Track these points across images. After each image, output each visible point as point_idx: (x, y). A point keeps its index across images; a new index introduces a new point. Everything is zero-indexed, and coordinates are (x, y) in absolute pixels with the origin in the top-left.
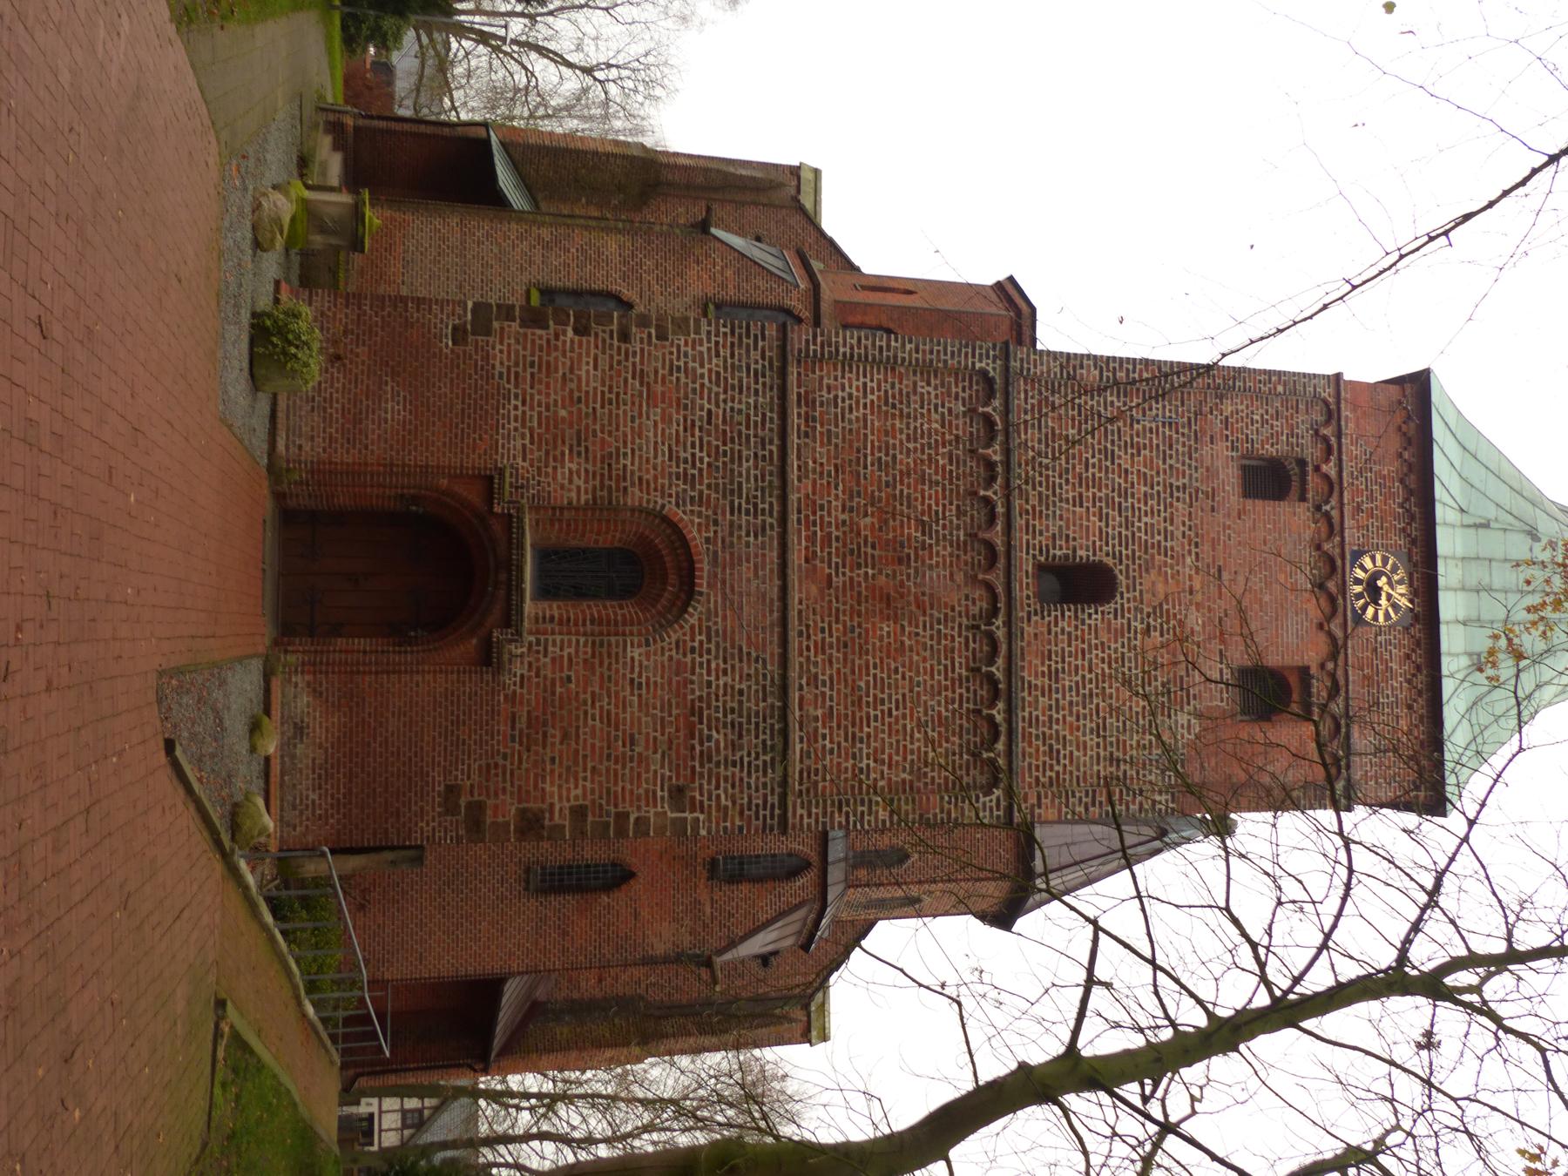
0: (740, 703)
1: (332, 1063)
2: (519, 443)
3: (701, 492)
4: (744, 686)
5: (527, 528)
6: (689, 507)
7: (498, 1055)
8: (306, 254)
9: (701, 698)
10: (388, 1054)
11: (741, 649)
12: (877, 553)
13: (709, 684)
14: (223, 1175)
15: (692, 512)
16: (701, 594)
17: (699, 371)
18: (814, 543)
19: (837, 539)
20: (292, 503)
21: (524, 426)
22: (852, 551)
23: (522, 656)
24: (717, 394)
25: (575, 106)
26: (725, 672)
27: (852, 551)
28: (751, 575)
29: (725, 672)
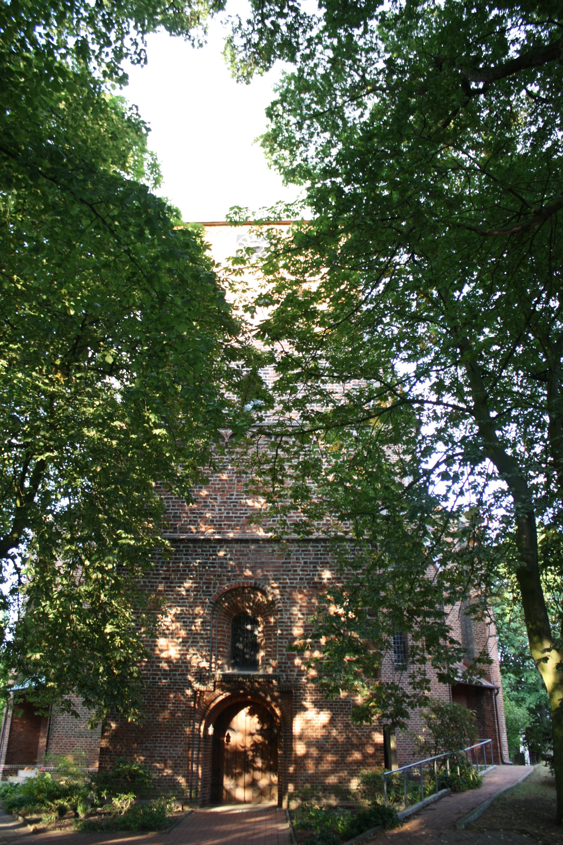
0: (311, 563)
1: (495, 768)
2: (178, 677)
3: (204, 583)
4: (302, 561)
5: (504, 726)
6: (211, 589)
7: (490, 681)
8: (273, 339)
9: (308, 583)
10: (490, 740)
11: (283, 563)
12: (235, 493)
13: (301, 579)
14: (1, 600)
15: (214, 588)
16: (255, 583)
17: (142, 583)
18: (230, 525)
19: (228, 513)
20: (208, 797)
21: (169, 675)
22: (234, 506)
23: (287, 675)
24: (154, 574)
25: (417, 661)
26: (295, 571)
27: (234, 506)
28: (246, 558)
29: (295, 571)
